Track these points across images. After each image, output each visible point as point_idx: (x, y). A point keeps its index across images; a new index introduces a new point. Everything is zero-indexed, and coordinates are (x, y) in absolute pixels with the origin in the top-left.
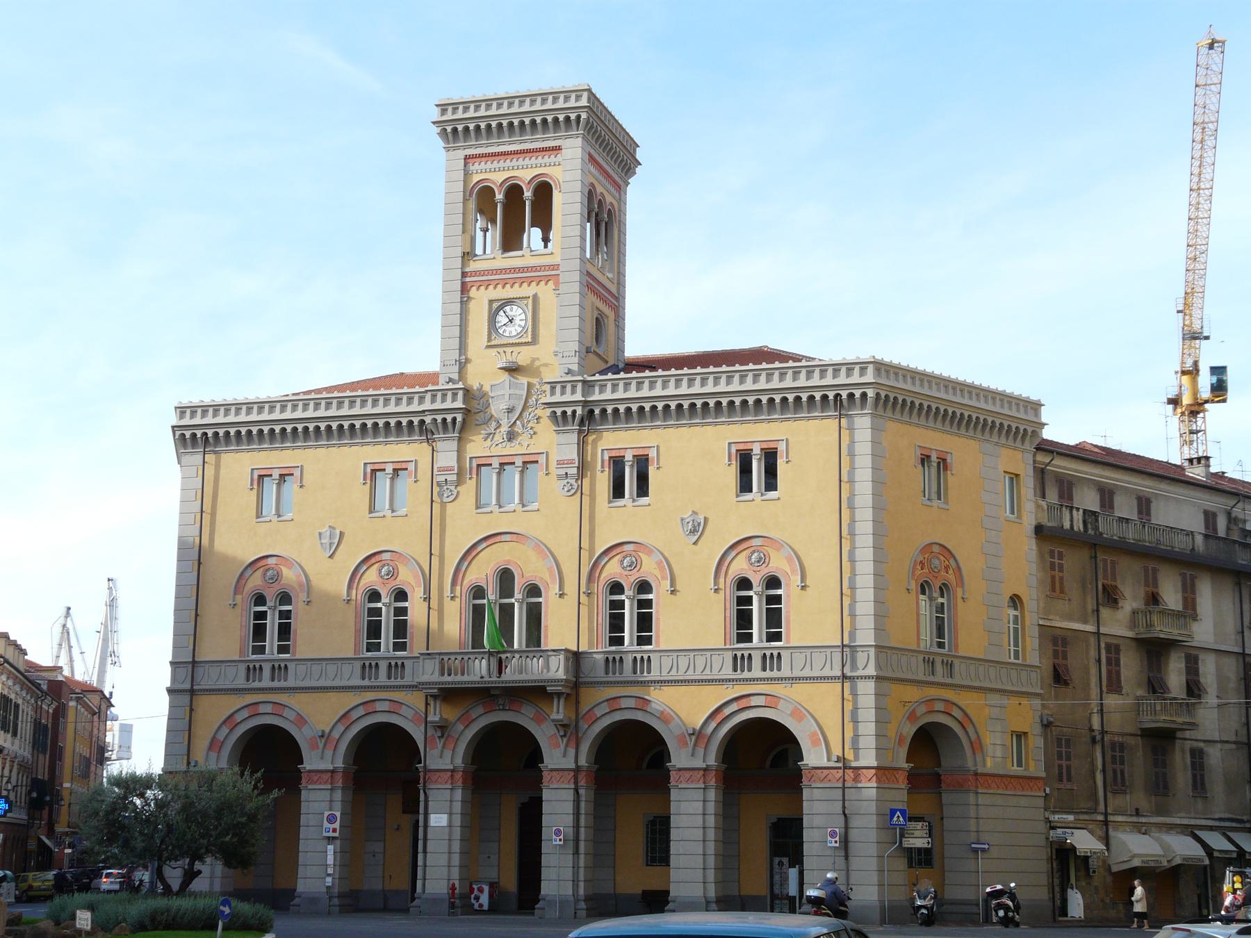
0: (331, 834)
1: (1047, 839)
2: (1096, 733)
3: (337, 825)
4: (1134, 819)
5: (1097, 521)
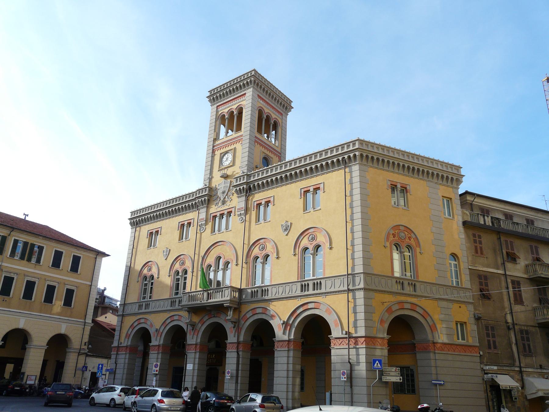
0: (156, 372)
1: (483, 379)
2: (510, 324)
3: (158, 369)
4: (539, 371)
5: (500, 222)
